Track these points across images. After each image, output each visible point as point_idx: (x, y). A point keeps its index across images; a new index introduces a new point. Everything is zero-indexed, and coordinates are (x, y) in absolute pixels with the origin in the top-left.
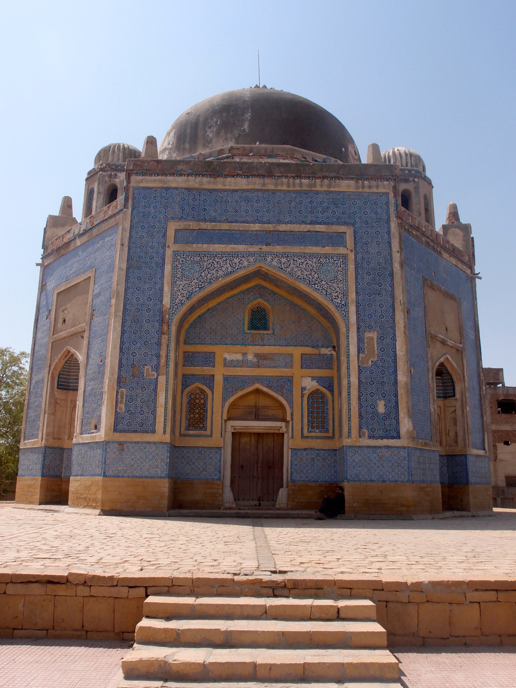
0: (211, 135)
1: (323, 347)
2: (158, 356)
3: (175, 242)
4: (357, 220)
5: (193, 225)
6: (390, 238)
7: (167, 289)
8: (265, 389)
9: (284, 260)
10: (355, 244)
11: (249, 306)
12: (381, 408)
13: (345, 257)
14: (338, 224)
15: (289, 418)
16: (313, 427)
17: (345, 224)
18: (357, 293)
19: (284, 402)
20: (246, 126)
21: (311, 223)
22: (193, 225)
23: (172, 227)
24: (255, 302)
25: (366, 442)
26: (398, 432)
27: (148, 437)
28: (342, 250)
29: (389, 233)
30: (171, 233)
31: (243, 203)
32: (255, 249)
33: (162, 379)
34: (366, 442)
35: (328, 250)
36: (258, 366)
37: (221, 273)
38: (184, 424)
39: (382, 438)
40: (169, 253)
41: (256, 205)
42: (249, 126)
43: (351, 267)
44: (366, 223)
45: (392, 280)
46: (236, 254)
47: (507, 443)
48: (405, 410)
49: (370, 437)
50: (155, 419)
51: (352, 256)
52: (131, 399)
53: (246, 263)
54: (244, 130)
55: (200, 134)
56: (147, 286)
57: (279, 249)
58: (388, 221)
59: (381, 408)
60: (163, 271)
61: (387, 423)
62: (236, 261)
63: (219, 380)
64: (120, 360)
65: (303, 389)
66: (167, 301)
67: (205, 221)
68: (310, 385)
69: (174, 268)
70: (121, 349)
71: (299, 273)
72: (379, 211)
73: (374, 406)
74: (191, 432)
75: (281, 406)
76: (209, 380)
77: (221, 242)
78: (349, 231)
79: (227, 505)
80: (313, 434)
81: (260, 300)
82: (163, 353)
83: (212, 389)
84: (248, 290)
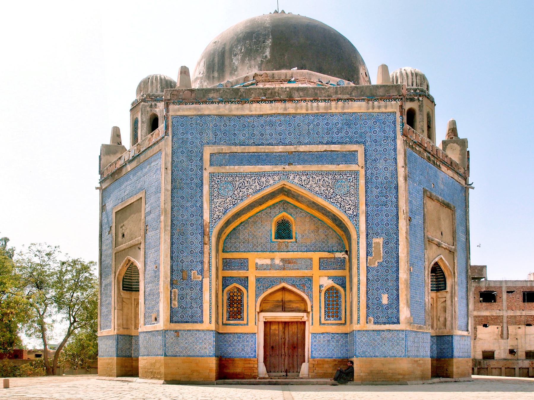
0: (236, 63)
1: (337, 251)
2: (202, 263)
3: (211, 165)
4: (368, 139)
5: (225, 149)
6: (396, 155)
7: (206, 206)
8: (290, 287)
9: (304, 178)
10: (366, 161)
11: (275, 219)
12: (385, 300)
13: (356, 173)
14: (351, 143)
15: (309, 310)
16: (329, 316)
17: (357, 143)
18: (366, 205)
19: (306, 297)
20: (268, 53)
21: (327, 143)
22: (225, 149)
23: (207, 151)
24: (280, 215)
25: (372, 326)
26: (398, 319)
27: (198, 326)
28: (354, 167)
29: (395, 150)
30: (206, 157)
31: (267, 127)
32: (279, 168)
33: (206, 281)
34: (372, 326)
35: (342, 167)
36: (284, 269)
37: (250, 191)
38: (225, 316)
39: (385, 323)
40: (206, 175)
41: (279, 128)
42: (270, 52)
43: (362, 182)
44: (375, 141)
45: (397, 192)
46: (263, 174)
47: (485, 326)
48: (405, 301)
49: (375, 323)
50: (202, 312)
51: (362, 172)
52: (182, 298)
53: (272, 182)
54: (266, 57)
55: (227, 62)
56: (189, 204)
57: (299, 168)
58: (395, 138)
59: (385, 300)
60: (202, 191)
61: (389, 311)
62: (263, 179)
63: (252, 281)
64: (172, 267)
65: (321, 286)
66: (206, 216)
67: (235, 144)
68: (327, 283)
69: (211, 187)
70: (172, 258)
71: (317, 189)
72: (387, 129)
73: (379, 299)
74: (232, 322)
75: (303, 300)
76: (245, 281)
77: (250, 163)
78: (360, 149)
79: (261, 376)
80: (329, 322)
81: (284, 214)
82: (206, 260)
83: (246, 287)
84: (274, 205)
